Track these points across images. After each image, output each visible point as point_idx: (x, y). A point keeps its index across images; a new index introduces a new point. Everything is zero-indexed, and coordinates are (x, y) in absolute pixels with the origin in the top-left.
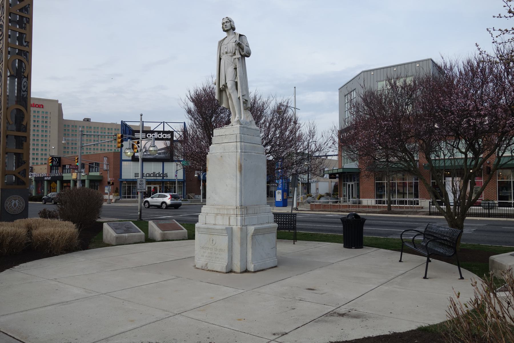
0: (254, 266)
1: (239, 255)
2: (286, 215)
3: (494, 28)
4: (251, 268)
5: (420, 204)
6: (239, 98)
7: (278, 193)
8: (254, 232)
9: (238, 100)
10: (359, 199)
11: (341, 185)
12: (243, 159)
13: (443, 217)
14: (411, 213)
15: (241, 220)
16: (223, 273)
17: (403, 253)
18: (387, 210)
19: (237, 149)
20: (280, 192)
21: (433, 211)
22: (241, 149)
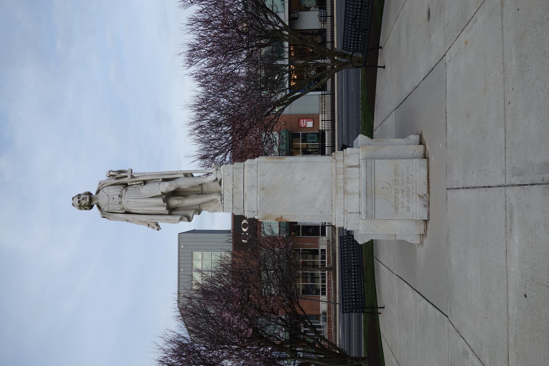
10: (319, 315)
13: (336, 74)
18: (331, 272)
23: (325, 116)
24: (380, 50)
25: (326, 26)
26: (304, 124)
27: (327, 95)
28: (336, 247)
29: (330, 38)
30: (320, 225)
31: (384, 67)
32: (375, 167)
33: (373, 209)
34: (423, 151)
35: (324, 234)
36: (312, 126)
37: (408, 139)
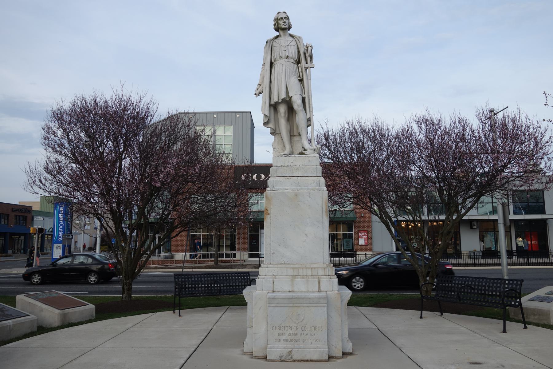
2: (220, 275)
7: (57, 248)
16: (325, 361)
18: (213, 264)
20: (59, 247)
24: (439, 313)
25: (464, 258)
28: (238, 268)
31: (421, 317)
32: (319, 307)
33: (277, 305)
34: (336, 356)
35: (251, 256)
36: (360, 244)
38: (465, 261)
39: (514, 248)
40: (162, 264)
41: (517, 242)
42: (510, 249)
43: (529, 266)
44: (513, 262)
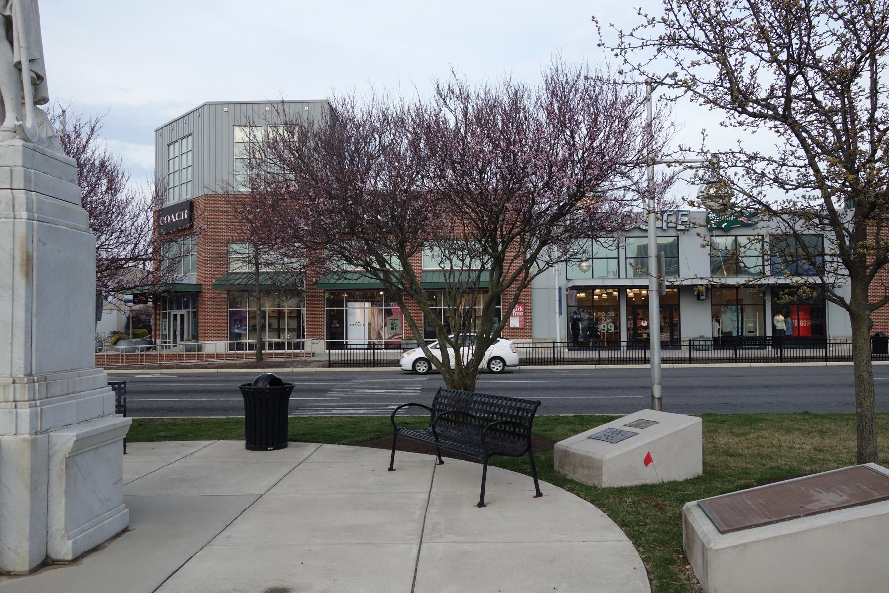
0: (74, 543)
1: (27, 521)
3: (640, 9)
4: (64, 549)
5: (306, 347)
6: (18, 66)
8: (74, 446)
9: (14, 70)
10: (197, 341)
11: (157, 316)
12: (35, 240)
14: (297, 365)
15: (33, 417)
17: (396, 452)
18: (254, 360)
19: (14, 210)
21: (379, 358)
22: (29, 210)
23: (528, 349)
25: (685, 349)
26: (516, 312)
27: (552, 351)
28: (294, 367)
29: (634, 357)
30: (345, 341)
34: (16, 570)
35: (330, 347)
36: (512, 326)
37: (62, 536)
38: (685, 354)
39: (769, 333)
40: (175, 360)
41: (775, 322)
42: (763, 335)
43: (781, 362)
44: (762, 356)
